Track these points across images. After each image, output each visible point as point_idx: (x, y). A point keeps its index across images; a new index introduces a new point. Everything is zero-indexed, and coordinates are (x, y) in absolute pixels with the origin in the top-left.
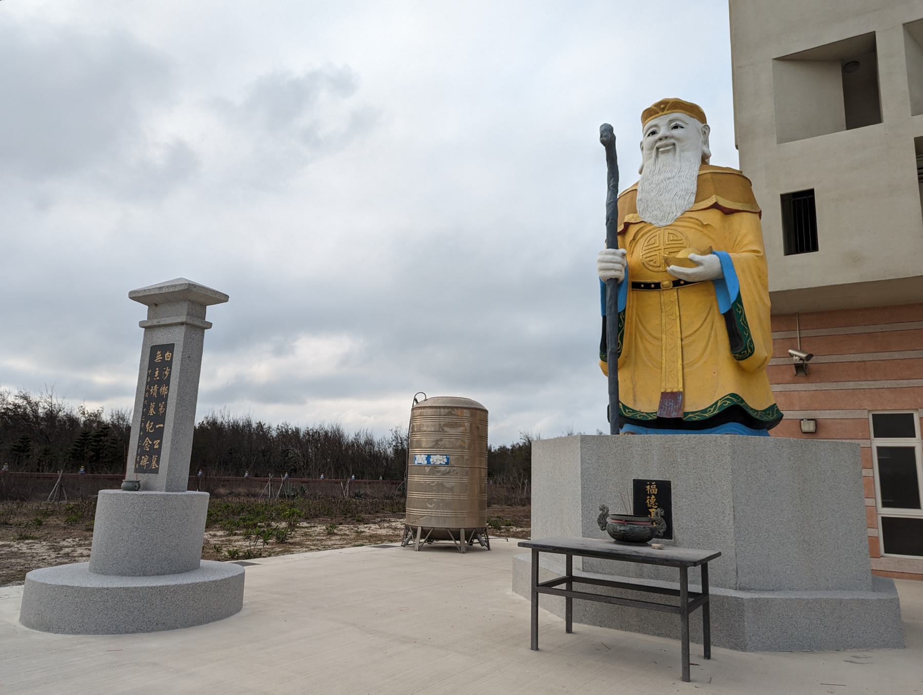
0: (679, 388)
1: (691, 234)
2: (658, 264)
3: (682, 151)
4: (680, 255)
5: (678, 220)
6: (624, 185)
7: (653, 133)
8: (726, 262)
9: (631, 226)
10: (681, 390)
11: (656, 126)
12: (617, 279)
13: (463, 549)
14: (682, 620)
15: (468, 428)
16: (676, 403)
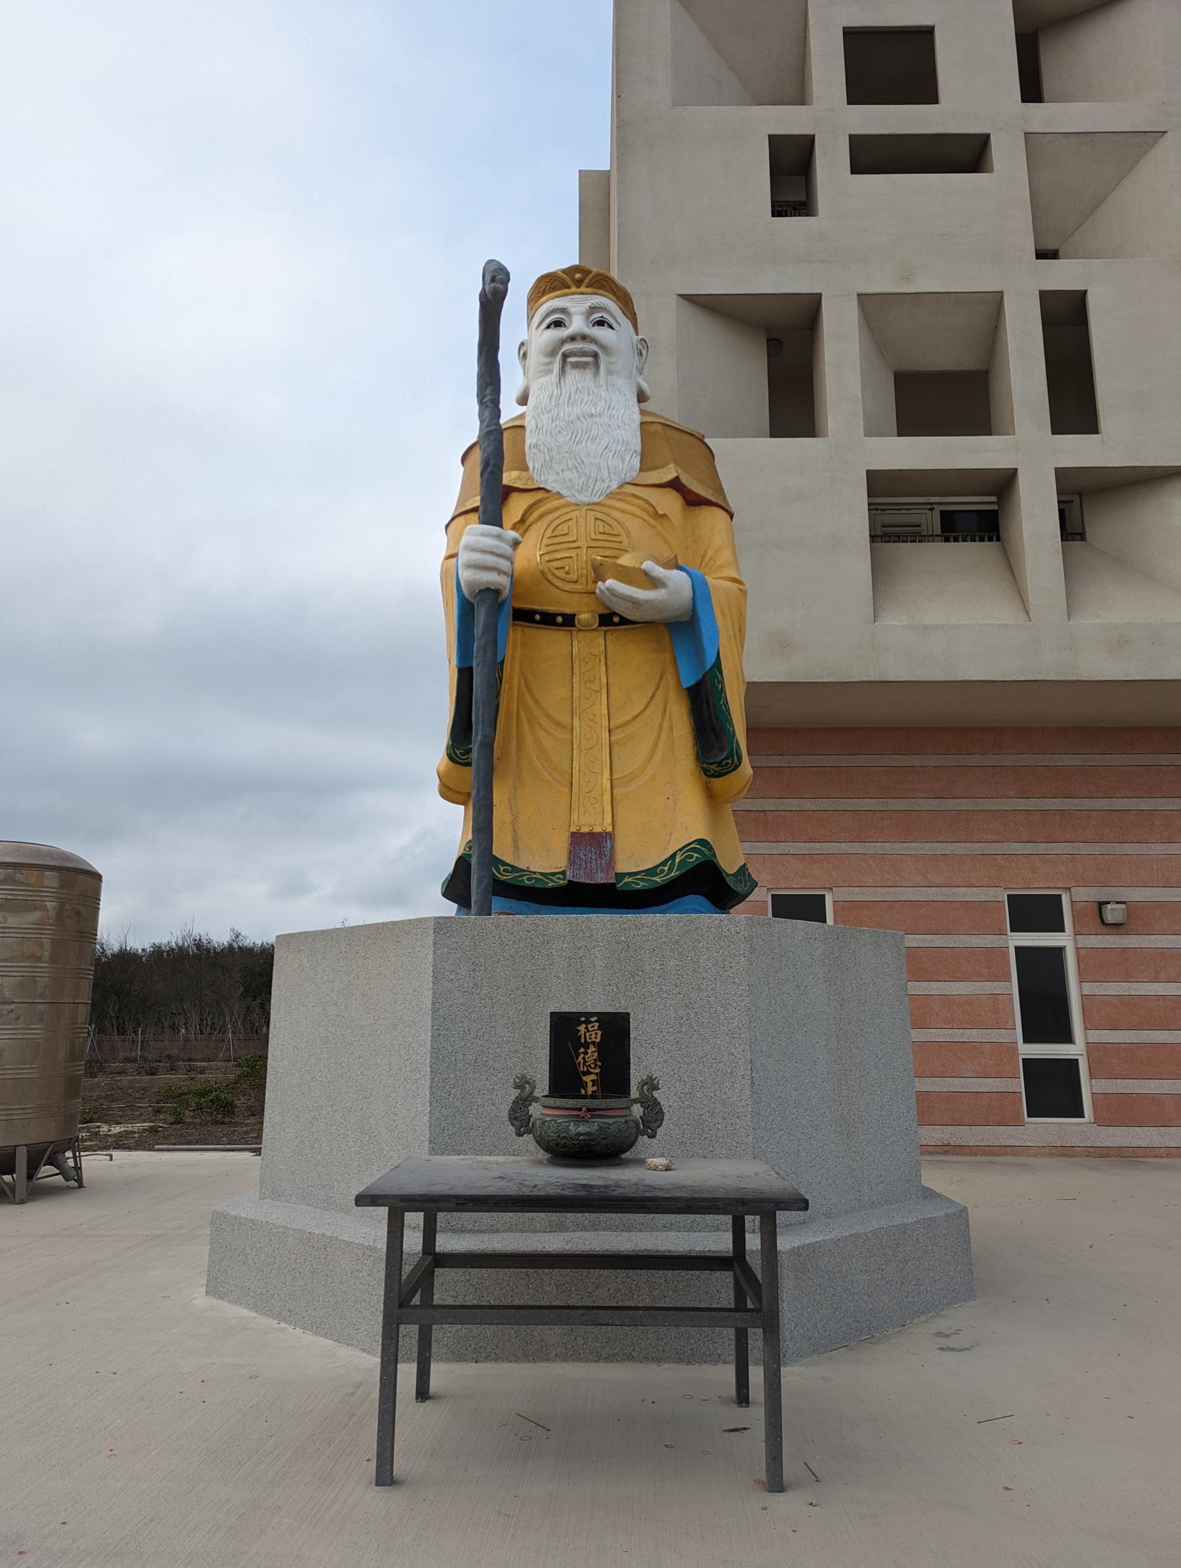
0: (603, 824)
1: (635, 526)
2: (574, 577)
3: (609, 372)
4: (625, 560)
5: (611, 495)
6: (509, 410)
7: (558, 324)
8: (699, 589)
9: (515, 496)
10: (609, 829)
11: (563, 310)
12: (497, 592)
13: (21, 1191)
14: (765, 1340)
15: (53, 914)
16: (601, 855)
